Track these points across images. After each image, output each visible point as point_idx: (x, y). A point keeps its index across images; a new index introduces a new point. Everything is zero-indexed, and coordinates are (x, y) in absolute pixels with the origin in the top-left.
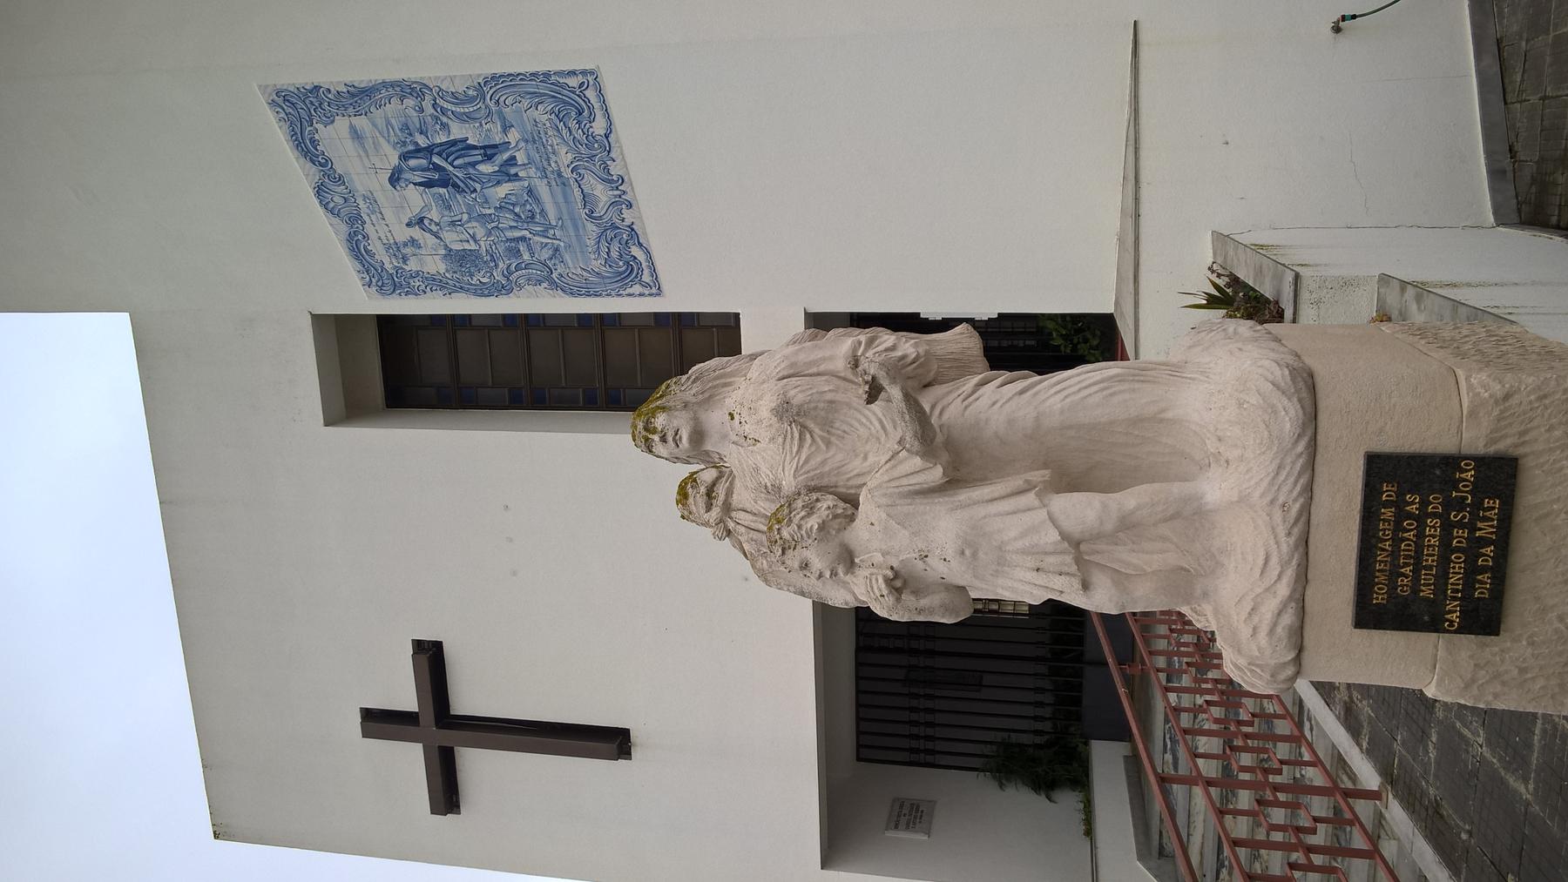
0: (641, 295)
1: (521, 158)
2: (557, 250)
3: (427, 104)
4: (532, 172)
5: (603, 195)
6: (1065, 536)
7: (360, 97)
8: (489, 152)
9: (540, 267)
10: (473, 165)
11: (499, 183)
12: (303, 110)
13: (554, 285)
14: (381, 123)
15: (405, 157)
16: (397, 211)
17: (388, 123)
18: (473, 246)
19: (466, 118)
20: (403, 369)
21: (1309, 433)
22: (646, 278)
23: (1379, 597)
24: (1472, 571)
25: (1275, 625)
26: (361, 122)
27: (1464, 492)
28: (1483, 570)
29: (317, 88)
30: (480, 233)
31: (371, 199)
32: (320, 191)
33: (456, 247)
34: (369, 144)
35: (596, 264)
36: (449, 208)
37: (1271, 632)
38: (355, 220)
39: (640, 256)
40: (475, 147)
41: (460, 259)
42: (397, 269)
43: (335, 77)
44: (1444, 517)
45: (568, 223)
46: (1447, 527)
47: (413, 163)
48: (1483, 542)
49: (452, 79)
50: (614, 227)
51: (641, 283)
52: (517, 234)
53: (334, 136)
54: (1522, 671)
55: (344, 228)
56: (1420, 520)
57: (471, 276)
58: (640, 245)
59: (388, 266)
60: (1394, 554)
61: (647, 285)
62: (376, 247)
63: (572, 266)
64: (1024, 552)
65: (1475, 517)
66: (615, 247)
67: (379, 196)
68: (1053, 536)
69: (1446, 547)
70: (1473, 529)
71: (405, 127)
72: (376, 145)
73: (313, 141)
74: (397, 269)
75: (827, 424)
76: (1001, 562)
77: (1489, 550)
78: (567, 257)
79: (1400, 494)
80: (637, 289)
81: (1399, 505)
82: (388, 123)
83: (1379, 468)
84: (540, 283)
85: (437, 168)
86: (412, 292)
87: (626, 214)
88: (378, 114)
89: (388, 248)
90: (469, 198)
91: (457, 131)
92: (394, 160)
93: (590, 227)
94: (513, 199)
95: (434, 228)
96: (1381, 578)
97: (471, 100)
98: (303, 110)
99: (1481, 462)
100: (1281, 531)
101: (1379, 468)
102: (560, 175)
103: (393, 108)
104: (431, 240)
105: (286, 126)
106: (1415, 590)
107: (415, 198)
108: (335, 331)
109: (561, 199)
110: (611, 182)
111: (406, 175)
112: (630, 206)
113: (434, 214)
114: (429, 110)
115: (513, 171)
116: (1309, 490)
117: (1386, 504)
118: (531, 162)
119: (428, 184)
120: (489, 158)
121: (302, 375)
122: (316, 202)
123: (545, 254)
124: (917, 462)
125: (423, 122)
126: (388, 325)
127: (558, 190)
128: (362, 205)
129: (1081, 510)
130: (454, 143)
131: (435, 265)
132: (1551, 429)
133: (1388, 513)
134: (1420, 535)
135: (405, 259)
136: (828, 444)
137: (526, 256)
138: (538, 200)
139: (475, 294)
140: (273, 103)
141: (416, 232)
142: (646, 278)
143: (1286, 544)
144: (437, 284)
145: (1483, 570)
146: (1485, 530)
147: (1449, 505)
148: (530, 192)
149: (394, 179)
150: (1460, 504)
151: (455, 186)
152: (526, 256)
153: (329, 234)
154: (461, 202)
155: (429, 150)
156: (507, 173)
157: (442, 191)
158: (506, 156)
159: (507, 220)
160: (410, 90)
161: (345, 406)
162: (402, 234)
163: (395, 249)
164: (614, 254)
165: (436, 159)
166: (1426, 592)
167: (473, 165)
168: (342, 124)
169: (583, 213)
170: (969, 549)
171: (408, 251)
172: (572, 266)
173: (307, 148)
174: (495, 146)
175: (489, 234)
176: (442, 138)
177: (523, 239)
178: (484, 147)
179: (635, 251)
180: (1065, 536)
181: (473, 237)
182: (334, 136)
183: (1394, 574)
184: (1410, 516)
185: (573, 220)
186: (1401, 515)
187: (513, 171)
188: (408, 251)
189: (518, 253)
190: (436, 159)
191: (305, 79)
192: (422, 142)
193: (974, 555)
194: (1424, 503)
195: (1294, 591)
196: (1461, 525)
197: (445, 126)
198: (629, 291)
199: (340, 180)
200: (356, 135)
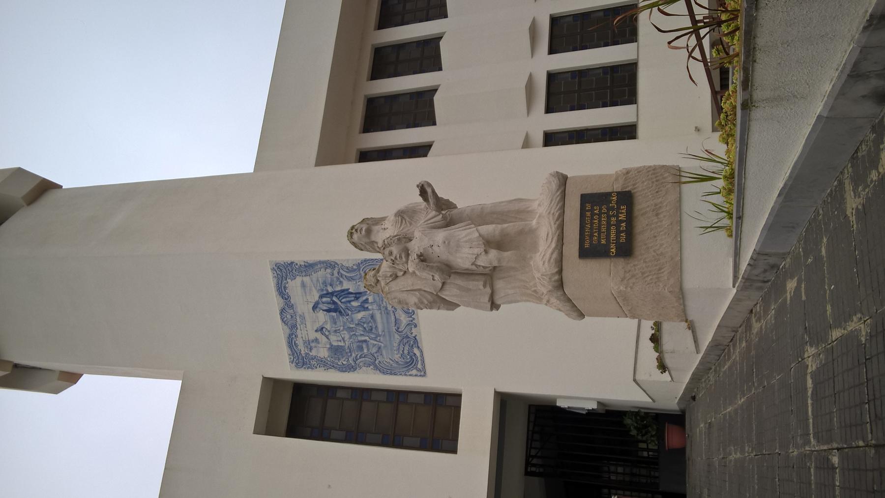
0: (416, 375)
1: (371, 299)
2: (380, 348)
3: (335, 272)
4: (375, 307)
5: (404, 319)
6: (480, 235)
7: (309, 268)
8: (357, 295)
9: (371, 356)
10: (350, 302)
11: (359, 311)
12: (284, 272)
13: (376, 368)
14: (315, 279)
15: (321, 297)
16: (313, 320)
17: (318, 280)
18: (342, 344)
19: (350, 279)
20: (300, 411)
21: (562, 188)
22: (419, 366)
23: (587, 245)
24: (618, 232)
25: (550, 258)
26: (307, 279)
27: (613, 205)
28: (622, 232)
29: (292, 263)
30: (347, 337)
31: (303, 317)
32: (282, 311)
33: (335, 344)
34: (308, 290)
35: (397, 357)
36: (335, 323)
37: (549, 260)
38: (293, 327)
39: (418, 354)
40: (352, 293)
41: (336, 350)
42: (307, 354)
43: (300, 258)
44: (607, 213)
45: (387, 334)
46: (609, 217)
47: (324, 300)
48: (622, 221)
49: (348, 260)
50: (407, 337)
51: (417, 369)
52: (363, 338)
53: (294, 286)
54: (643, 273)
55: (288, 331)
56: (600, 215)
57: (339, 360)
58: (418, 347)
59: (303, 352)
60: (592, 228)
61: (419, 370)
62: (300, 342)
63: (386, 358)
64: (466, 242)
65: (618, 213)
66: (407, 348)
67: (307, 315)
68: (477, 234)
69: (609, 225)
70: (618, 217)
71: (325, 283)
72: (310, 290)
73: (285, 287)
74: (307, 354)
75: (411, 218)
76: (458, 246)
77: (624, 224)
78: (384, 352)
79: (592, 207)
80: (414, 372)
81: (592, 210)
82: (318, 280)
83: (585, 199)
84: (369, 365)
85: (334, 303)
86: (311, 367)
87: (414, 330)
88: (314, 276)
89: (305, 342)
90: (345, 318)
91: (346, 285)
92: (317, 298)
93: (397, 336)
94: (364, 320)
95: (327, 333)
96: (587, 238)
97: (353, 270)
98: (284, 272)
99: (618, 193)
100: (552, 223)
101: (585, 199)
102: (386, 309)
103: (321, 273)
104: (324, 339)
105: (275, 280)
106: (599, 241)
107: (322, 317)
108: (272, 386)
109: (385, 321)
110: (408, 313)
111: (320, 306)
112: (416, 326)
113: (328, 326)
114: (336, 274)
115: (366, 306)
116: (563, 207)
117: (588, 211)
118: (375, 301)
119: (329, 311)
120: (357, 298)
121: (249, 404)
122: (279, 316)
123: (374, 350)
124: (434, 213)
125: (332, 280)
126: (300, 389)
127: (384, 316)
128: (298, 320)
129: (488, 229)
130: (343, 291)
131: (323, 352)
132: (643, 182)
133: (588, 214)
134: (600, 221)
135: (311, 349)
136: (411, 224)
137: (365, 351)
138: (375, 321)
139: (339, 370)
140: (273, 269)
141: (318, 335)
142: (419, 366)
143: (554, 227)
144: (324, 364)
145: (622, 232)
146: (622, 217)
147: (608, 209)
148: (372, 317)
149: (315, 308)
150: (613, 209)
151: (340, 312)
152: (365, 351)
153: (280, 332)
154: (342, 320)
155: (332, 294)
156: (362, 307)
157: (334, 314)
158: (364, 298)
159: (360, 331)
160: (330, 265)
161: (267, 426)
162: (313, 335)
163: (308, 344)
164: (406, 352)
165: (335, 299)
166: (603, 242)
167: (350, 302)
168: (299, 280)
169: (394, 329)
170: (447, 242)
171: (313, 345)
172: (386, 358)
173: (282, 291)
174: (360, 293)
175: (350, 338)
176: (338, 288)
177: (365, 341)
178: (356, 294)
179: (416, 351)
180: (480, 235)
181: (343, 339)
182: (294, 286)
183: (591, 236)
184: (596, 214)
185: (389, 332)
186: (593, 215)
187: (366, 306)
188: (313, 345)
189: (361, 349)
190: (335, 299)
191: (288, 259)
192: (330, 289)
193: (449, 243)
194: (600, 209)
195: (557, 245)
196: (613, 216)
197: (341, 283)
198: (410, 373)
199: (291, 307)
200: (303, 285)
